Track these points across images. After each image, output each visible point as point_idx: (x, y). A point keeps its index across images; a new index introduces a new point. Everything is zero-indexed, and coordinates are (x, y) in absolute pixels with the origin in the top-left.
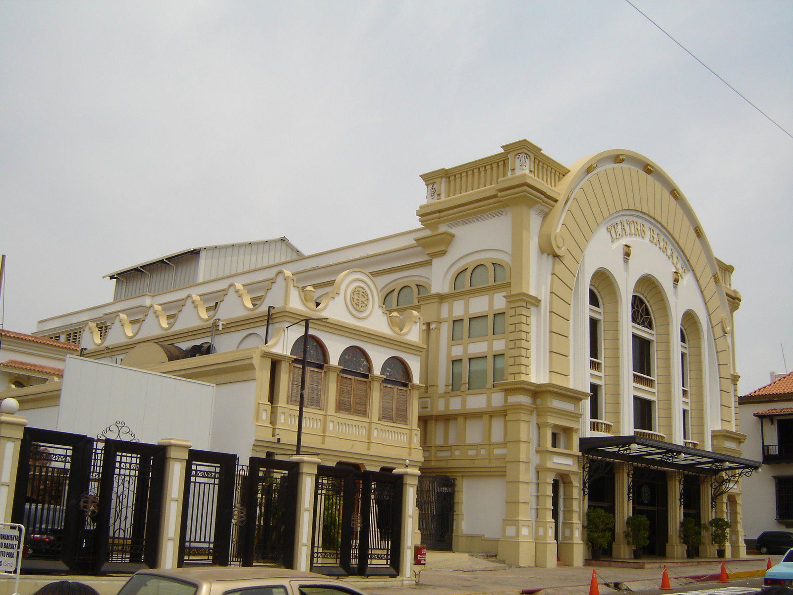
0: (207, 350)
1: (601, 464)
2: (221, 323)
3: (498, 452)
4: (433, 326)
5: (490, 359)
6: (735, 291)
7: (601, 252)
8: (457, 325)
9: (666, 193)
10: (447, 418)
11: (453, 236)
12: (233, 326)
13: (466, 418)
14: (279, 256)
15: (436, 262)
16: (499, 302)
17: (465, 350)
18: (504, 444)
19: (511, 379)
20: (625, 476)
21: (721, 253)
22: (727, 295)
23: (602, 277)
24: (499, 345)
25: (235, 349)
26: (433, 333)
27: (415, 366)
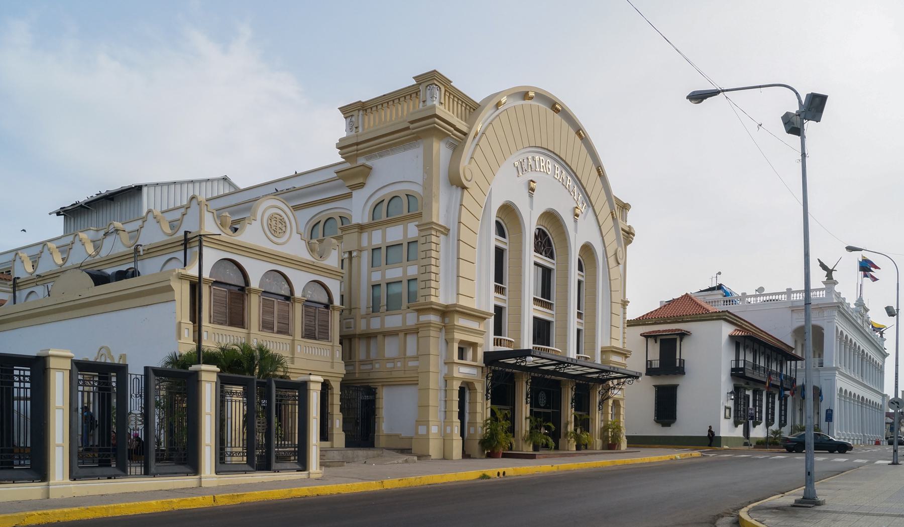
0: (134, 273)
1: (502, 373)
2: (141, 249)
3: (411, 364)
4: (354, 254)
5: (405, 283)
6: (629, 227)
7: (505, 187)
8: (376, 252)
9: (572, 133)
10: (369, 336)
11: (370, 168)
12: (154, 251)
13: (384, 336)
14: (223, 189)
15: (356, 194)
16: (413, 231)
17: (383, 275)
18: (416, 358)
19: (422, 300)
20: (524, 384)
21: (618, 191)
22: (623, 230)
23: (509, 210)
24: (413, 271)
25: (158, 271)
26: (354, 260)
27: (335, 287)
